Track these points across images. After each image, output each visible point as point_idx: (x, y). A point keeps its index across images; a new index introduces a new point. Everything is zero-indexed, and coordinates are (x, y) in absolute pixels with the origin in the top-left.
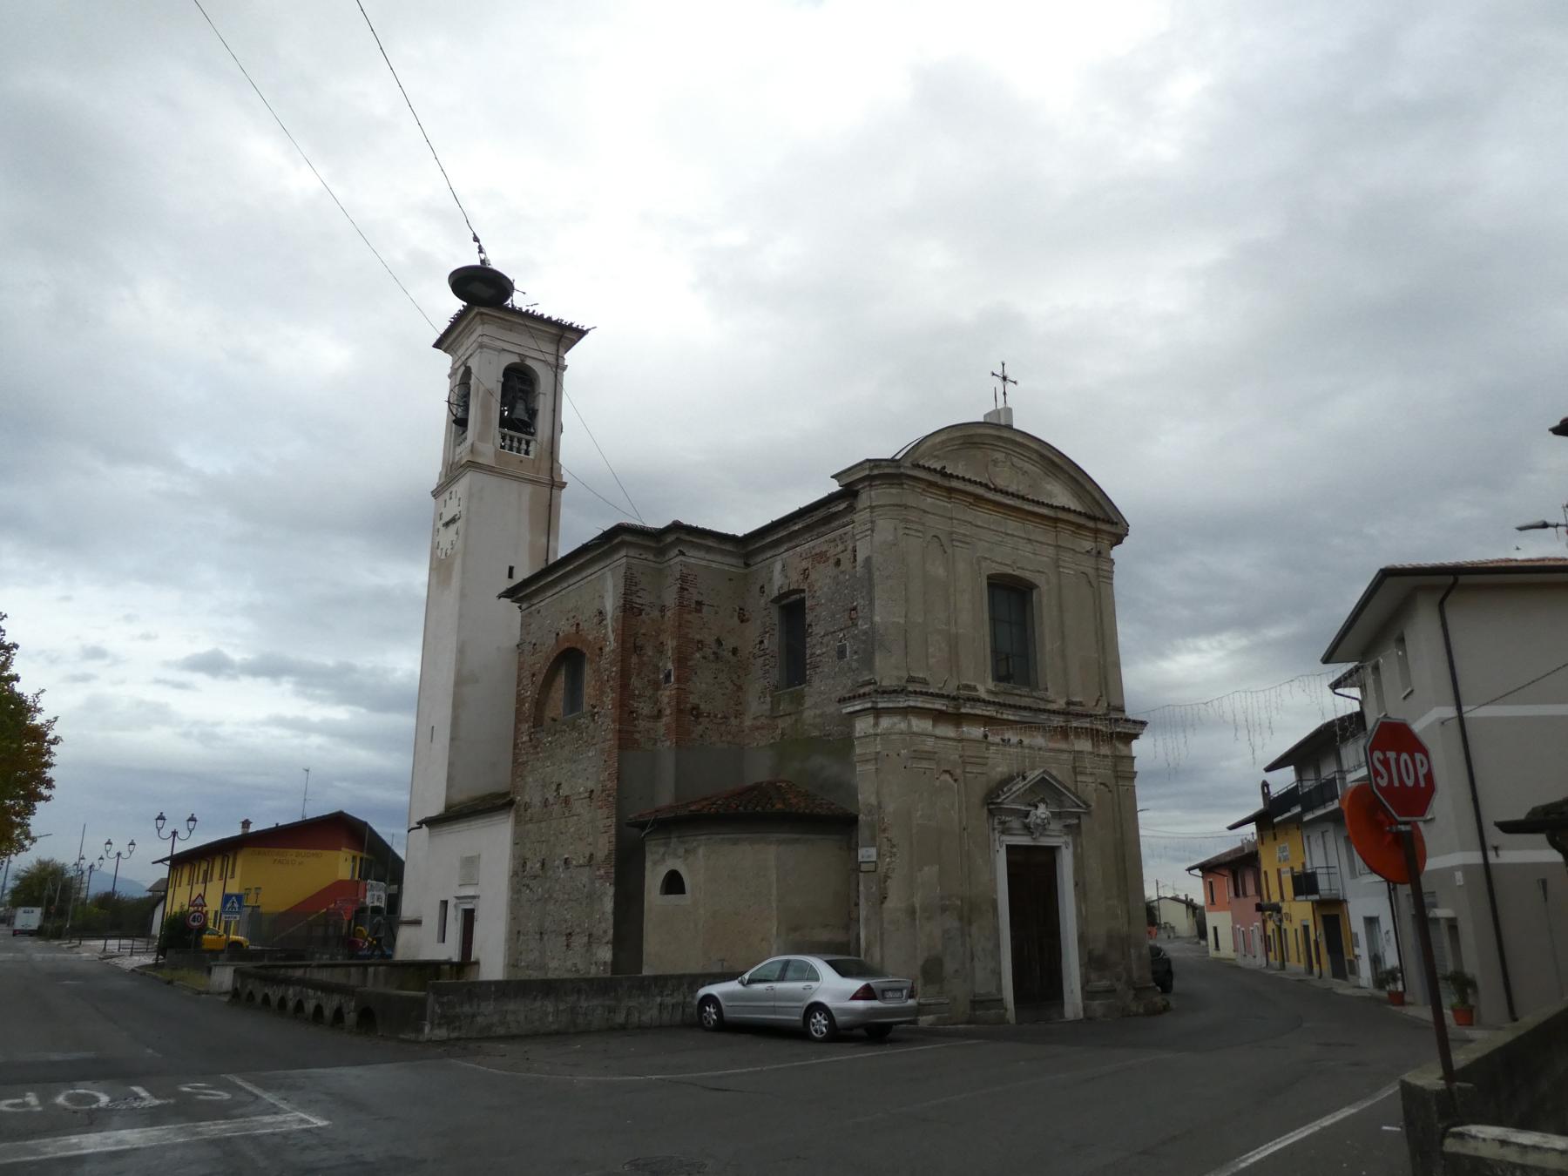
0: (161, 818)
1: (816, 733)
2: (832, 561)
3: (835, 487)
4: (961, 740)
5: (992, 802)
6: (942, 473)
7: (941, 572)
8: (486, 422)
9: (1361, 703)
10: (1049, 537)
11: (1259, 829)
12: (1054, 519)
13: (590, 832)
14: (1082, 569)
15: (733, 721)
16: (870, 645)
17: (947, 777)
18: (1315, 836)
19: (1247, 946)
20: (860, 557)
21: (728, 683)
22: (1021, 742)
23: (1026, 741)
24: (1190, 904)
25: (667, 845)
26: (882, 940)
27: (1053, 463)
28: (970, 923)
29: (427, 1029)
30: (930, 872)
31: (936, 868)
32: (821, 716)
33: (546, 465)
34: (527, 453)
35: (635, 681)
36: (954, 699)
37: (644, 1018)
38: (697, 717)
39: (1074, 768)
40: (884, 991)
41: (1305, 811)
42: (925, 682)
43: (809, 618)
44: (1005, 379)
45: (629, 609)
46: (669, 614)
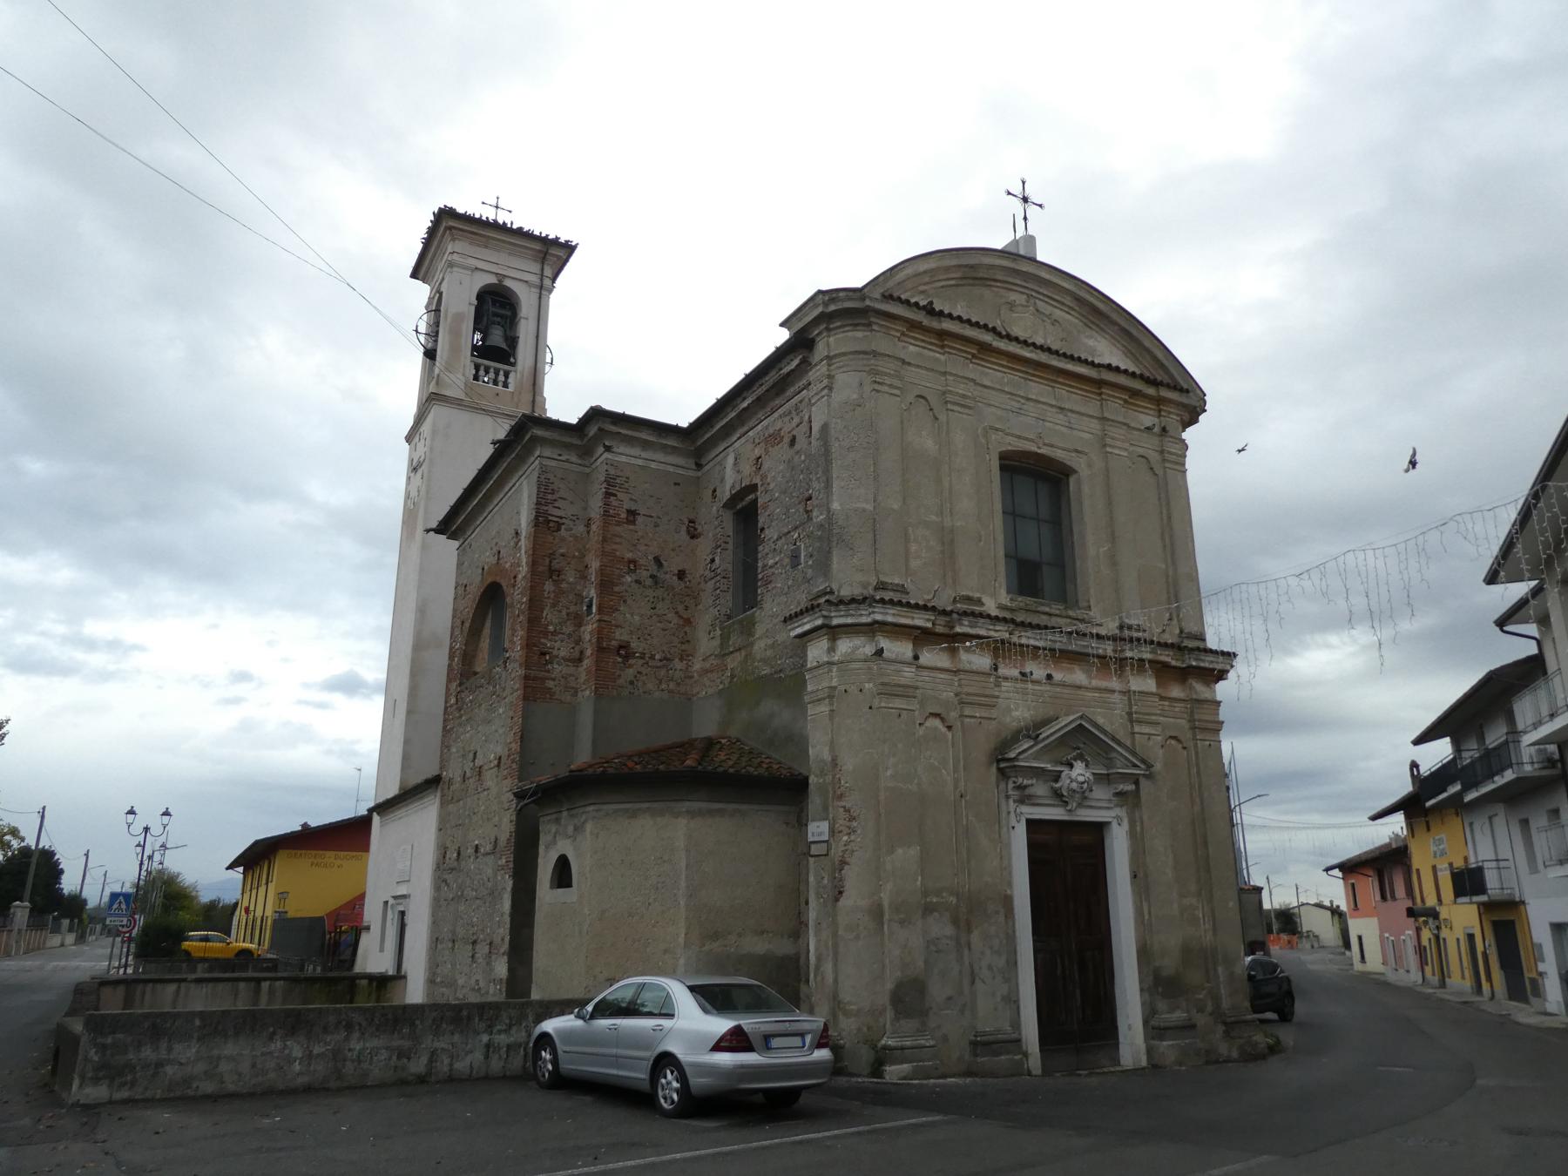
0: (132, 812)
1: (766, 671)
2: (787, 440)
3: (784, 335)
4: (956, 672)
5: (1003, 763)
6: (930, 310)
7: (930, 444)
8: (455, 350)
9: (1539, 643)
10: (1092, 407)
11: (1408, 817)
12: (1098, 382)
13: (495, 813)
14: (1141, 451)
15: (678, 664)
16: (828, 538)
17: (937, 722)
18: (1480, 823)
19: (1398, 959)
20: (816, 427)
21: (671, 616)
22: (1049, 677)
23: (1058, 676)
24: (1335, 912)
25: (557, 821)
26: (836, 954)
28: (969, 931)
29: (75, 1087)
30: (907, 855)
31: (914, 851)
32: (773, 646)
33: (527, 397)
34: (506, 385)
35: (548, 614)
36: (944, 613)
37: (458, 1065)
38: (627, 657)
39: (1130, 714)
40: (767, 1038)
41: (1466, 788)
42: (902, 589)
43: (762, 520)
44: (1025, 200)
45: (544, 522)
46: (594, 527)
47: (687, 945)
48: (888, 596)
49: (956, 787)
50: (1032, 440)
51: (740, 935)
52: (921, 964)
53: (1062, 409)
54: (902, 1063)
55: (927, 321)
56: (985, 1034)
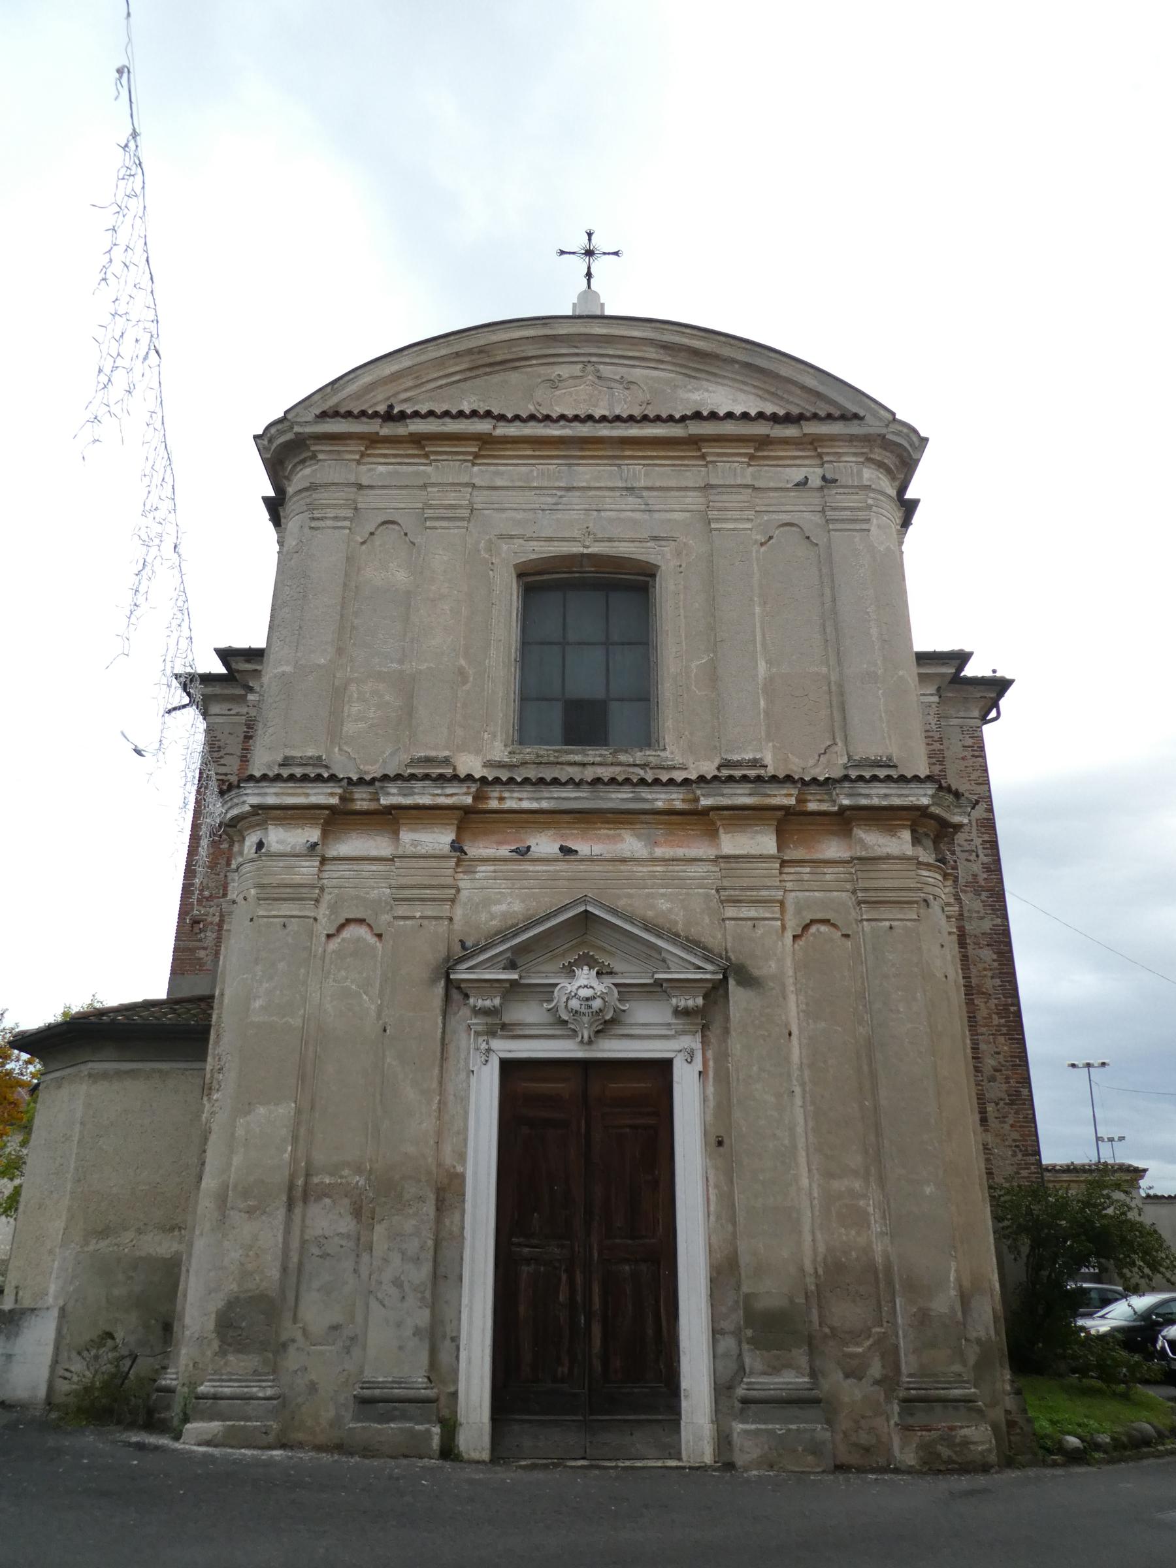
7: (401, 577)
12: (691, 439)
23: (583, 848)
27: (696, 353)
31: (285, 1110)
47: (64, 1244)
48: (298, 771)
49: (379, 1017)
50: (574, 540)
51: (139, 1231)
52: (274, 1273)
53: (632, 489)
54: (211, 1419)
55: (386, 430)
56: (372, 1385)
